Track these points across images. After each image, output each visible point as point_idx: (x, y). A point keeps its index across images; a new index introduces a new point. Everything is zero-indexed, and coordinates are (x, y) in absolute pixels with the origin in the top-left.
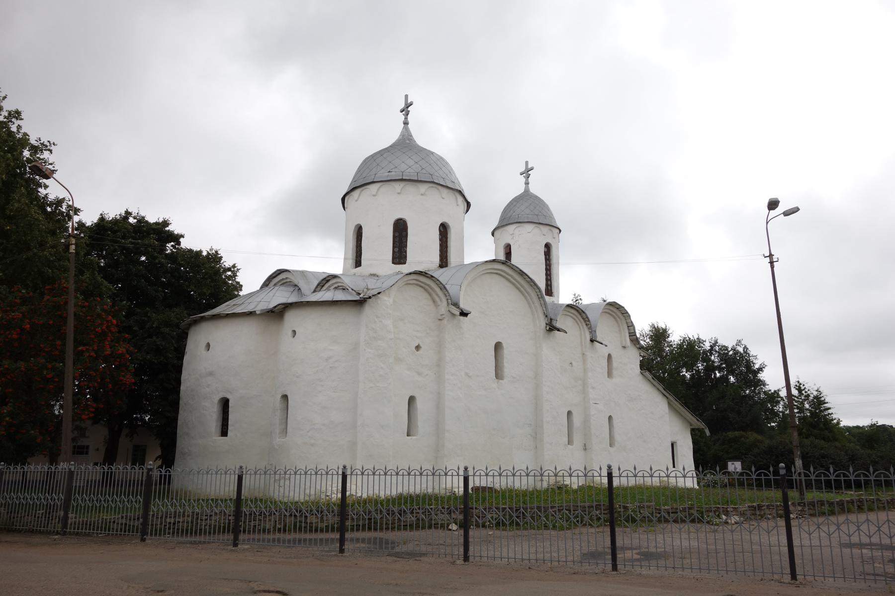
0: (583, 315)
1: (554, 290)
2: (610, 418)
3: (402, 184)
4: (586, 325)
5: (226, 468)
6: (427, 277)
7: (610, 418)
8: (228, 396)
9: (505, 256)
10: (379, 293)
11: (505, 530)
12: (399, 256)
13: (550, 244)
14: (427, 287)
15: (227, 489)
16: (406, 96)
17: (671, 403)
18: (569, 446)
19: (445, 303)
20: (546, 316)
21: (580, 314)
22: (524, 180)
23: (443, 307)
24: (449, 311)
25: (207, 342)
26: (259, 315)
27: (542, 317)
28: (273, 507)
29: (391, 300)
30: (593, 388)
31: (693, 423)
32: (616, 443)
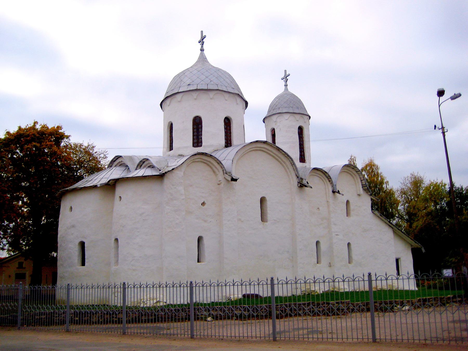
0: (327, 175)
1: (306, 158)
2: (349, 244)
3: (198, 93)
4: (329, 181)
5: (153, 283)
6: (208, 156)
7: (349, 244)
8: (84, 240)
9: (272, 136)
10: (173, 169)
11: (254, 320)
12: (197, 141)
13: (303, 127)
14: (208, 163)
15: (88, 298)
16: (202, 32)
17: (396, 231)
18: (318, 264)
19: (222, 173)
20: (298, 177)
21: (324, 174)
22: (284, 83)
23: (221, 176)
24: (224, 178)
25: (70, 206)
26: (99, 187)
27: (295, 178)
28: (108, 308)
29: (182, 173)
30: (335, 224)
31: (413, 244)
32: (353, 261)
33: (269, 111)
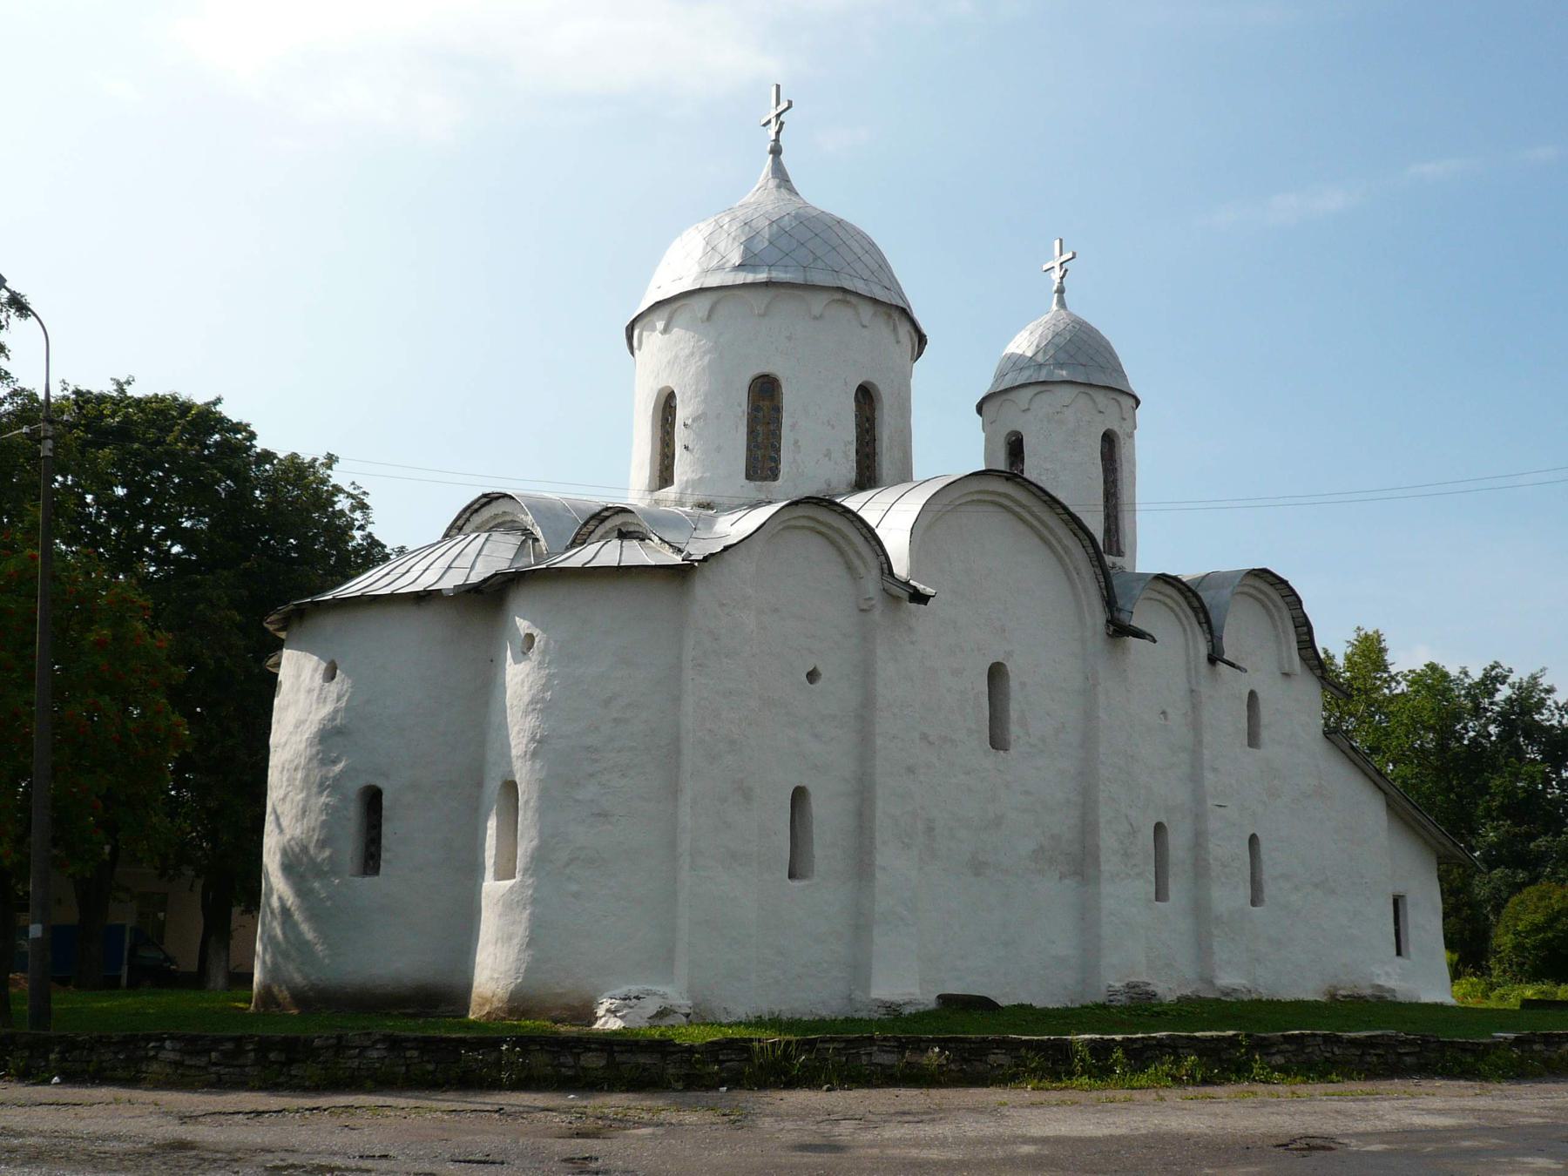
2: (1253, 840)
3: (772, 292)
19: (875, 573)
30: (1215, 770)
33: (1001, 375)
